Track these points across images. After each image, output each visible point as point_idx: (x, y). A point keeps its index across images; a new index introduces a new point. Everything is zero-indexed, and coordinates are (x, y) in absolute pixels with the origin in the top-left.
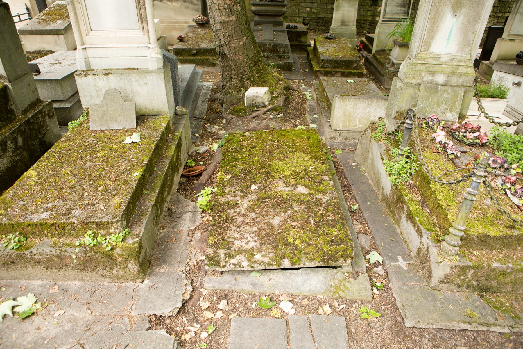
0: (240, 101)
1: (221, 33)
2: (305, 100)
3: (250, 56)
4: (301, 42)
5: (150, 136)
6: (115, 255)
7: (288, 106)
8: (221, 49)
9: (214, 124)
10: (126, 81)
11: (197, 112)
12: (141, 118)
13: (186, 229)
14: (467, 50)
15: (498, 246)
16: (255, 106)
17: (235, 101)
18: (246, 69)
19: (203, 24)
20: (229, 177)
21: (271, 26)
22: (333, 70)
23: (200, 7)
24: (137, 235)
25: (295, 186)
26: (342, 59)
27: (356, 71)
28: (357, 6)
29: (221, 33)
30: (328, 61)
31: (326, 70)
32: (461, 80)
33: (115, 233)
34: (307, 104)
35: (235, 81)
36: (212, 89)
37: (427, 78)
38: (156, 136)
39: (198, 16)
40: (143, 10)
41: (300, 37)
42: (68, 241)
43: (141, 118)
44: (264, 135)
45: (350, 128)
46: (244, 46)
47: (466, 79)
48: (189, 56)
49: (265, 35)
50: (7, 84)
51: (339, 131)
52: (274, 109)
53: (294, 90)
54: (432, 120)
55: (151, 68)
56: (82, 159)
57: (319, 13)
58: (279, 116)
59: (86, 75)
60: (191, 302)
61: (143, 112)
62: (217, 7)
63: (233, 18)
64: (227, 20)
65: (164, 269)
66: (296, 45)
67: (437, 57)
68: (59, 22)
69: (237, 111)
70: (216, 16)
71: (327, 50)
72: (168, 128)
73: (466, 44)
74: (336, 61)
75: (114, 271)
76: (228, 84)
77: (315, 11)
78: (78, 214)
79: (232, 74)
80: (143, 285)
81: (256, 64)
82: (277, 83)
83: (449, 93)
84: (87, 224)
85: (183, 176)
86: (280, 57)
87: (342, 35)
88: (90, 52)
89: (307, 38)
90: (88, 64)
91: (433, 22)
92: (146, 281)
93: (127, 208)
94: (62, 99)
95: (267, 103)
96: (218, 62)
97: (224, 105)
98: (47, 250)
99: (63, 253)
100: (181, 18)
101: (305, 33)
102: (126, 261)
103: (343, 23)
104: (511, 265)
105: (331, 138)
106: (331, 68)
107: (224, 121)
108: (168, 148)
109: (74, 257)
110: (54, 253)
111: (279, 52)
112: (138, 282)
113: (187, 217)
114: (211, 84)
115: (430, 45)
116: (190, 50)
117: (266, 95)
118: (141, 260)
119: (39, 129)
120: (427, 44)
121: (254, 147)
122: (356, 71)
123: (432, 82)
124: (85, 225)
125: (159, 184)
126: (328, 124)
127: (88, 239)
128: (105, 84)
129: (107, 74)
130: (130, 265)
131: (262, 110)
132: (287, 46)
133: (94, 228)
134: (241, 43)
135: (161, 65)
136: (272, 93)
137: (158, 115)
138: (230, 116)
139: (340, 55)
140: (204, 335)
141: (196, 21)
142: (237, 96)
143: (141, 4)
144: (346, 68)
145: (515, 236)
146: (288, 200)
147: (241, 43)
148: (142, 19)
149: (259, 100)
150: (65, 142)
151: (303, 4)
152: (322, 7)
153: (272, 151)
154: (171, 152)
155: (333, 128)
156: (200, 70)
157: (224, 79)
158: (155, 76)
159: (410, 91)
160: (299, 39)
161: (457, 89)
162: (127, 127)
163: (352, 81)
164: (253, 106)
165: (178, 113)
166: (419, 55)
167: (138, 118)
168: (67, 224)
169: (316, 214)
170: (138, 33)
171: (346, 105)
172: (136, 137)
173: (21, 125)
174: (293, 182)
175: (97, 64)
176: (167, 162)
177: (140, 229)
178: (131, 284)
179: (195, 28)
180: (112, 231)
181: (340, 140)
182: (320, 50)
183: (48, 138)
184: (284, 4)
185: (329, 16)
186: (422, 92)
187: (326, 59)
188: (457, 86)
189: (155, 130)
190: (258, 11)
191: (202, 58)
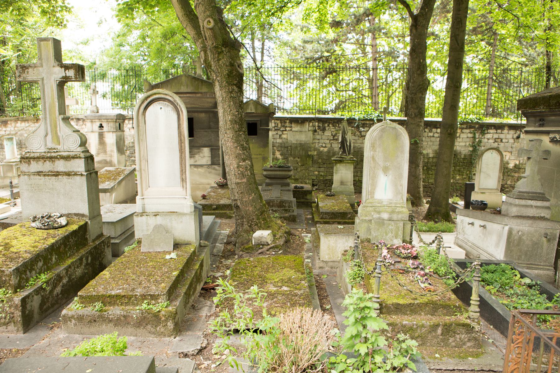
0: (249, 241)
1: (236, 191)
2: (304, 243)
3: (258, 208)
4: (307, 199)
5: (183, 255)
6: (161, 315)
7: (289, 244)
8: (235, 202)
9: (229, 259)
10: (168, 220)
11: (215, 251)
12: (177, 246)
13: (204, 314)
14: (400, 196)
15: (408, 312)
16: (261, 244)
17: (245, 241)
18: (254, 217)
19: (223, 186)
20: (236, 283)
21: (280, 186)
22: (331, 220)
23: (221, 172)
24: (175, 306)
25: (281, 287)
26: (338, 211)
27: (350, 221)
28: (352, 169)
29: (236, 191)
30: (326, 213)
31: (325, 220)
32: (400, 216)
33: (162, 302)
34: (305, 247)
35: (246, 227)
36: (228, 236)
37: (376, 216)
38: (187, 256)
39: (219, 179)
40: (184, 175)
41: (306, 195)
42: (131, 308)
43: (177, 246)
44: (263, 259)
45: (334, 259)
46: (253, 200)
47: (403, 215)
48: (210, 210)
49: (274, 194)
50: (87, 220)
51: (326, 262)
52: (276, 247)
53: (295, 236)
54: (381, 244)
55: (185, 212)
56: (137, 266)
57: (326, 176)
58: (280, 252)
59: (141, 216)
60: (206, 350)
61: (177, 242)
62: (233, 173)
63: (245, 180)
64: (240, 181)
65: (190, 333)
66: (303, 202)
67: (380, 202)
68: (107, 183)
69: (246, 249)
70: (232, 179)
71: (325, 204)
72: (194, 252)
73: (397, 193)
74: (333, 213)
75: (158, 329)
76: (241, 229)
77: (322, 174)
78: (139, 291)
79: (243, 221)
80: (175, 339)
81: (262, 213)
82: (279, 229)
83: (392, 226)
84: (145, 296)
85: (203, 289)
86: (286, 210)
87: (341, 193)
88: (146, 201)
89: (312, 196)
90: (144, 208)
91: (373, 180)
92: (177, 338)
93: (169, 290)
94: (113, 236)
95: (270, 242)
96: (234, 215)
97: (237, 245)
98: (118, 312)
99: (128, 314)
100: (204, 181)
101: (310, 192)
102: (166, 320)
103: (342, 183)
104: (415, 323)
105: (320, 268)
106: (330, 219)
107: (236, 257)
108: (195, 265)
109: (135, 316)
110: (122, 314)
111: (285, 207)
112: (172, 338)
113: (206, 309)
114: (228, 232)
115: (374, 194)
116: (211, 205)
117: (269, 236)
118: (176, 320)
119: (100, 254)
120: (372, 193)
121: (256, 266)
122: (350, 221)
123: (379, 218)
124: (144, 297)
125: (189, 283)
126: (318, 258)
127: (144, 306)
128: (153, 221)
129: (156, 215)
130: (169, 324)
131: (266, 248)
132: (291, 202)
133: (148, 299)
134: (250, 198)
135: (193, 209)
136: (274, 236)
137: (188, 244)
138: (241, 253)
139: (336, 208)
140: (214, 365)
141: (217, 183)
142: (247, 238)
143: (184, 171)
144: (342, 219)
145: (417, 304)
146: (275, 294)
147: (250, 198)
148: (183, 180)
149: (264, 240)
150: (124, 257)
151: (311, 169)
152: (328, 170)
153: (268, 269)
154: (197, 267)
155: (321, 260)
156: (219, 221)
157: (237, 225)
158: (188, 217)
159: (365, 225)
160: (305, 197)
161: (398, 222)
162: (167, 250)
163: (342, 227)
164: (259, 245)
165: (202, 245)
166: (368, 201)
167: (174, 246)
168: (133, 295)
169: (292, 300)
170: (179, 189)
171: (329, 241)
172: (173, 255)
173: (92, 249)
174: (280, 284)
175: (149, 209)
176: (194, 272)
177: (177, 303)
178: (167, 339)
179: (216, 188)
180: (159, 301)
181: (327, 268)
182: (320, 205)
183: (105, 261)
184: (290, 169)
185: (330, 177)
186: (373, 226)
187: (324, 211)
188: (398, 221)
189: (186, 252)
190: (269, 175)
191: (221, 212)
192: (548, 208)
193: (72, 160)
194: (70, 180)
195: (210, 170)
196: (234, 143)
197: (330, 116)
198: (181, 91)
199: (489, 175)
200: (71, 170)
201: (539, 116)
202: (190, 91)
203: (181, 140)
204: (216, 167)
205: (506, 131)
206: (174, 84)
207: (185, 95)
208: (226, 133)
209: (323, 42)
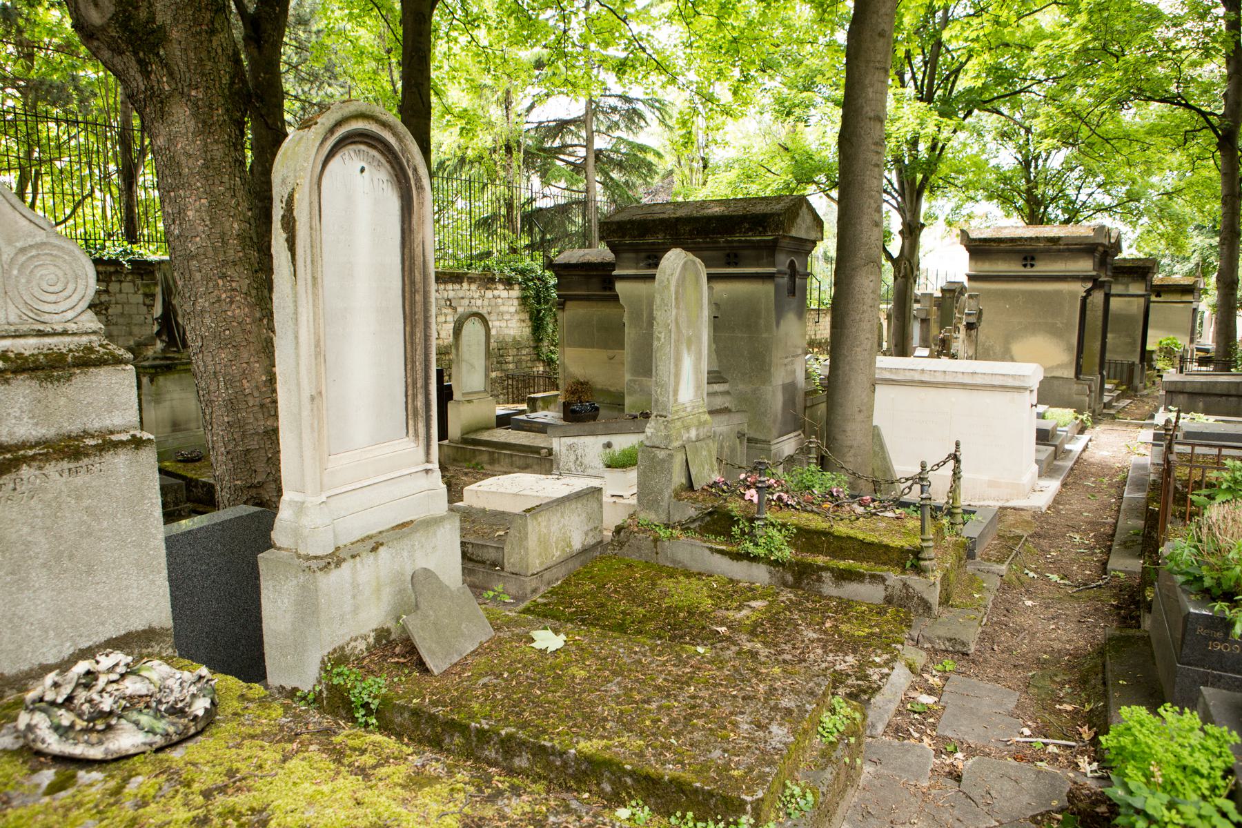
45: (549, 563)
192: (728, 393)
193: (80, 379)
194: (79, 480)
196: (251, 306)
199: (472, 366)
200: (74, 428)
201: (646, 250)
203: (413, 283)
205: (465, 285)
208: (223, 276)
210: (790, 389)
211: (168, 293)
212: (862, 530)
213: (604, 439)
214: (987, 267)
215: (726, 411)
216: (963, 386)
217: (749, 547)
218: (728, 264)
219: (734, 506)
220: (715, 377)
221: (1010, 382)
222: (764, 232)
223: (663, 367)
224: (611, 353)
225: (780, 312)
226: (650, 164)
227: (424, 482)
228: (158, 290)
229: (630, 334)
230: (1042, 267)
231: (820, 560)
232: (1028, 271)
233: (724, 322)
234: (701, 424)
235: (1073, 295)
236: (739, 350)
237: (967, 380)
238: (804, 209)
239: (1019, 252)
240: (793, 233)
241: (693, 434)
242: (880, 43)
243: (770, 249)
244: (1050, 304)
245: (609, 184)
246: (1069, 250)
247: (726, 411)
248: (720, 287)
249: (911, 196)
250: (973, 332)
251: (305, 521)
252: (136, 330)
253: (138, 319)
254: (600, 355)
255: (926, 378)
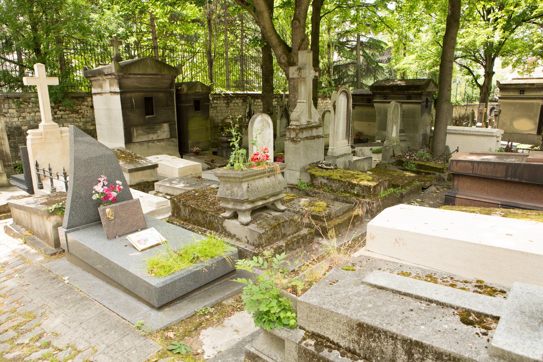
195: (169, 143)
197: (434, 118)
198: (148, 72)
202: (154, 72)
204: (174, 139)
206: (141, 66)
207: (148, 76)
209: (333, 26)
210: (425, 136)
211: (250, 106)
212: (432, 164)
213: (370, 148)
214: (506, 94)
215: (405, 141)
216: (475, 135)
217: (406, 167)
218: (408, 99)
219: (404, 159)
220: (402, 131)
221: (489, 134)
222: (418, 90)
223: (389, 129)
224: (369, 123)
225: (422, 113)
226: (382, 47)
227: (348, 147)
228: (248, 105)
229: (378, 118)
230: (527, 94)
231: (422, 171)
232: (522, 96)
233: (405, 115)
234: (397, 142)
235: (538, 104)
236: (408, 125)
237: (477, 133)
238: (431, 83)
239: (519, 89)
240: (427, 90)
241: (395, 144)
242: (452, 41)
243: (420, 95)
244: (529, 107)
245: (365, 56)
246: (538, 88)
247: (405, 141)
248: (404, 106)
249: (490, 60)
250: (497, 118)
251: (334, 151)
252: (224, 114)
253: (224, 111)
254: (366, 124)
255: (465, 133)
